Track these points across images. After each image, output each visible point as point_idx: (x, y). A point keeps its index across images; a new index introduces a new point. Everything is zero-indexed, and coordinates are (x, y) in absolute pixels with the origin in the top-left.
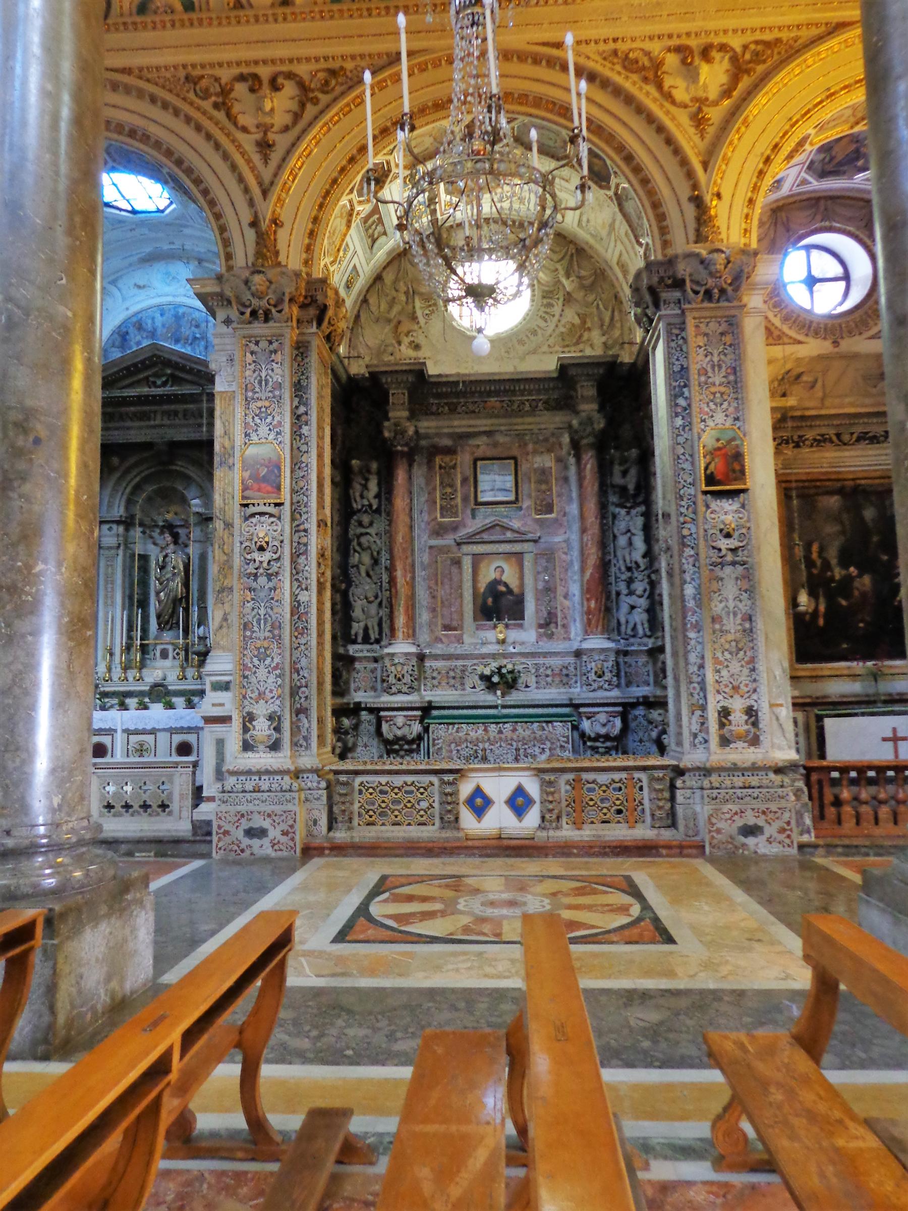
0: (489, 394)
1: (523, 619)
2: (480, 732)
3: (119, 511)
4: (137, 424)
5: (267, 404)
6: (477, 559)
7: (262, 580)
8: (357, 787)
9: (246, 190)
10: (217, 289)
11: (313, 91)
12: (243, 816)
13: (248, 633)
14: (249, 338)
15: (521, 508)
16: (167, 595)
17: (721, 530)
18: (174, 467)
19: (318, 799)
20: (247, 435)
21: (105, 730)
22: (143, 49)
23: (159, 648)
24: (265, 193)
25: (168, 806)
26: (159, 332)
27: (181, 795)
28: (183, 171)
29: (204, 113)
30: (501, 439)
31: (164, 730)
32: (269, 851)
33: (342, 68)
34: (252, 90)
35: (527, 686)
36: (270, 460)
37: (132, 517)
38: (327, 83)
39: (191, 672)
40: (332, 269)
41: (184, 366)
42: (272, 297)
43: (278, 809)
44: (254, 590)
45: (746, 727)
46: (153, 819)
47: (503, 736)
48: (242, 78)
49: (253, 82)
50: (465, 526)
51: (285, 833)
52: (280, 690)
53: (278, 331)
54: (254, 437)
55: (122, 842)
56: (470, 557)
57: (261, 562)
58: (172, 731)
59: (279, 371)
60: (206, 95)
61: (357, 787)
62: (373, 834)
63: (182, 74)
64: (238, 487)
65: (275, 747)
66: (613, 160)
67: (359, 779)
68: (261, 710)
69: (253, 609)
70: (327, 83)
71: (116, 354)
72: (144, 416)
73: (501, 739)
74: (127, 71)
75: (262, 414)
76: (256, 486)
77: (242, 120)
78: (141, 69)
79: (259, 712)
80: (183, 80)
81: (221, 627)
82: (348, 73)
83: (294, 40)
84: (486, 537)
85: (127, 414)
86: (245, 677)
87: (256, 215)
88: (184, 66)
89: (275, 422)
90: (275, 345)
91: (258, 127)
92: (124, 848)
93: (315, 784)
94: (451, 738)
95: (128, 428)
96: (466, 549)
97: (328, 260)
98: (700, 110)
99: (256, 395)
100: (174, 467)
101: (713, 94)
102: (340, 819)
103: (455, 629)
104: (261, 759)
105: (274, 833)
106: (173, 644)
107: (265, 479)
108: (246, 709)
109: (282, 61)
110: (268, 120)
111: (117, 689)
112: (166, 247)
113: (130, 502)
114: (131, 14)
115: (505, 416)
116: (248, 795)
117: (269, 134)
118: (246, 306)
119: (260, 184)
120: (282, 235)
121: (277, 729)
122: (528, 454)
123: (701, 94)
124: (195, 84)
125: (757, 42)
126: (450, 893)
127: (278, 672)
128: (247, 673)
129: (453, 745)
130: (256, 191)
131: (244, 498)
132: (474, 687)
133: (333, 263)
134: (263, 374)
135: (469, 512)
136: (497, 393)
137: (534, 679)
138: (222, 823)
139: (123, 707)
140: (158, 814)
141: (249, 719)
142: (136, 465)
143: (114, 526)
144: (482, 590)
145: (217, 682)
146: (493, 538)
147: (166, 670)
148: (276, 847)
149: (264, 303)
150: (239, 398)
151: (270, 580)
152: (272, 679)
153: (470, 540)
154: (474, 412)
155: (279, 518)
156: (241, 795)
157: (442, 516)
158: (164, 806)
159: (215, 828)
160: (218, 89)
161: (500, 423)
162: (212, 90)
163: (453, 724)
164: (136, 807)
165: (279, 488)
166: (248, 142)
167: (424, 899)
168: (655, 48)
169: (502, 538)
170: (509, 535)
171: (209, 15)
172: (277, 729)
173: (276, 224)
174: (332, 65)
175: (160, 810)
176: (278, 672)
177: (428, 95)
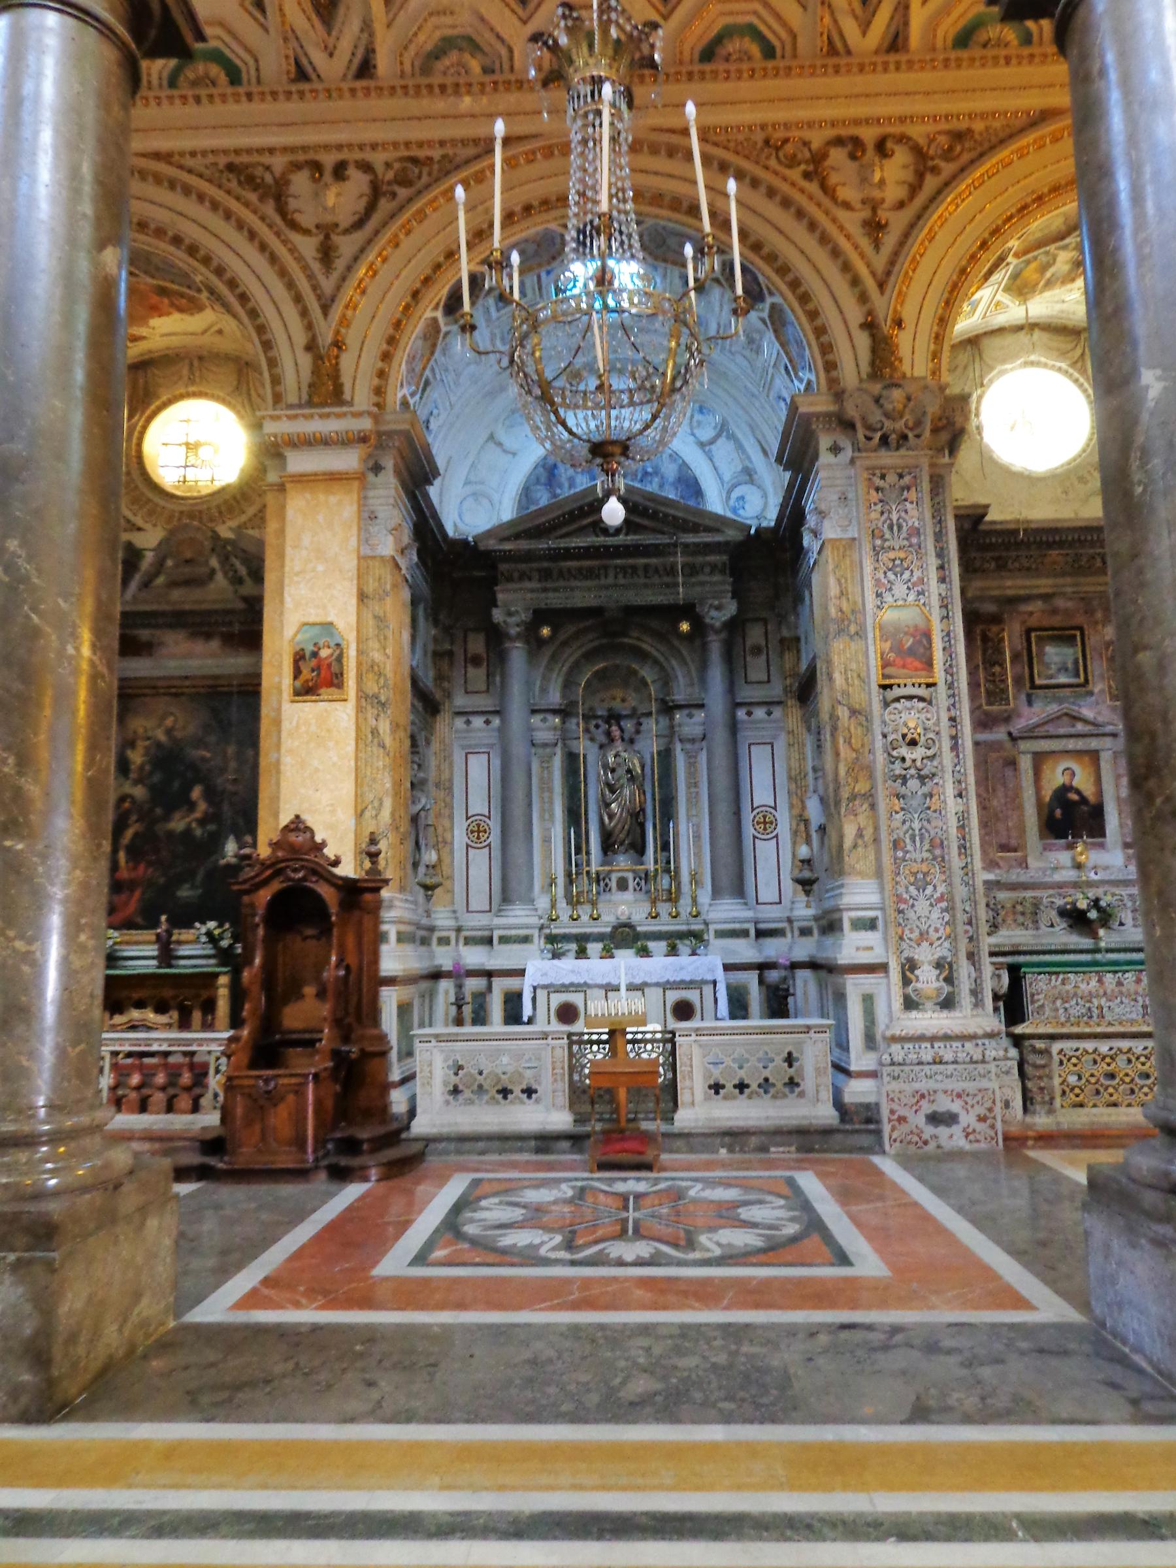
0: (1050, 545)
1: (1103, 835)
2: (1094, 983)
3: (555, 697)
5: (902, 555)
6: (1039, 759)
7: (913, 784)
8: (1056, 1058)
9: (855, 282)
10: (832, 408)
11: (932, 159)
12: (923, 1096)
13: (900, 854)
14: (871, 470)
15: (1091, 693)
16: (622, 807)
17: (904, 736)
18: (626, 640)
19: (1007, 1073)
20: (879, 595)
21: (579, 985)
23: (614, 877)
24: (325, 309)
27: (817, 1070)
28: (762, 258)
29: (793, 184)
30: (1060, 603)
31: (657, 984)
32: (961, 1142)
33: (970, 131)
34: (853, 157)
35: (1121, 924)
36: (916, 627)
37: (573, 704)
38: (951, 149)
39: (664, 908)
41: (646, 509)
42: (908, 417)
43: (970, 1086)
44: (903, 797)
45: (936, 985)
46: (778, 1102)
47: (1124, 989)
48: (839, 141)
49: (855, 146)
50: (1019, 716)
51: (982, 1119)
52: (948, 929)
53: (911, 462)
54: (888, 598)
55: (754, 1133)
56: (1029, 756)
57: (914, 761)
58: (667, 986)
59: (915, 513)
60: (792, 162)
61: (1056, 1058)
62: (1085, 1119)
63: (759, 137)
64: (874, 662)
65: (948, 1003)
66: (766, 274)
67: (1056, 1047)
68: (925, 955)
69: (904, 822)
70: (951, 149)
71: (543, 499)
72: (590, 574)
73: (1121, 993)
74: (157, 156)
75: (896, 568)
76: (899, 662)
77: (843, 193)
78: (182, 154)
79: (922, 958)
80: (760, 144)
81: (855, 846)
82: (977, 136)
84: (1051, 729)
85: (569, 570)
86: (900, 912)
87: (870, 313)
88: (763, 127)
89: (915, 579)
90: (907, 480)
91: (863, 202)
92: (754, 1141)
93: (1001, 1053)
94: (1056, 992)
96: (1024, 745)
98: (327, 237)
99: (887, 544)
100: (626, 640)
101: (345, 219)
102: (1039, 1099)
103: (1015, 850)
104: (930, 1021)
105: (967, 1119)
106: (634, 871)
107: (911, 651)
108: (905, 954)
109: (350, 146)
110: (876, 194)
111: (567, 931)
113: (568, 685)
114: (691, 61)
115: (1070, 575)
116: (927, 1068)
117: (879, 212)
118: (875, 430)
119: (873, 274)
120: (346, 362)
121: (949, 980)
122: (1096, 623)
123: (329, 218)
124: (777, 149)
125: (402, 159)
127: (944, 904)
128: (902, 906)
129: (1059, 1003)
130: (870, 284)
131: (884, 676)
132: (1052, 926)
134: (895, 517)
135: (1023, 697)
136: (1061, 544)
137: (1130, 915)
138: (895, 1107)
139: (582, 954)
140: (785, 1096)
141: (910, 966)
142: (576, 636)
143: (550, 717)
144: (1047, 799)
145: (859, 919)
146: (1062, 731)
147: (626, 906)
148: (971, 1137)
149: (900, 425)
150: (867, 548)
151: (923, 784)
152: (936, 914)
153: (1030, 734)
154: (1028, 569)
155: (930, 703)
156: (917, 1068)
157: (989, 703)
158: (529, 1092)
159: (885, 1113)
160: (807, 155)
161: (1067, 584)
162: (800, 156)
163: (1057, 973)
164: (754, 1086)
165: (929, 664)
166: (852, 221)
168: (279, 163)
169: (1072, 731)
170: (1080, 727)
172: (949, 980)
173: (340, 348)
174: (955, 125)
175: (787, 1090)
176: (944, 904)
177: (533, 192)
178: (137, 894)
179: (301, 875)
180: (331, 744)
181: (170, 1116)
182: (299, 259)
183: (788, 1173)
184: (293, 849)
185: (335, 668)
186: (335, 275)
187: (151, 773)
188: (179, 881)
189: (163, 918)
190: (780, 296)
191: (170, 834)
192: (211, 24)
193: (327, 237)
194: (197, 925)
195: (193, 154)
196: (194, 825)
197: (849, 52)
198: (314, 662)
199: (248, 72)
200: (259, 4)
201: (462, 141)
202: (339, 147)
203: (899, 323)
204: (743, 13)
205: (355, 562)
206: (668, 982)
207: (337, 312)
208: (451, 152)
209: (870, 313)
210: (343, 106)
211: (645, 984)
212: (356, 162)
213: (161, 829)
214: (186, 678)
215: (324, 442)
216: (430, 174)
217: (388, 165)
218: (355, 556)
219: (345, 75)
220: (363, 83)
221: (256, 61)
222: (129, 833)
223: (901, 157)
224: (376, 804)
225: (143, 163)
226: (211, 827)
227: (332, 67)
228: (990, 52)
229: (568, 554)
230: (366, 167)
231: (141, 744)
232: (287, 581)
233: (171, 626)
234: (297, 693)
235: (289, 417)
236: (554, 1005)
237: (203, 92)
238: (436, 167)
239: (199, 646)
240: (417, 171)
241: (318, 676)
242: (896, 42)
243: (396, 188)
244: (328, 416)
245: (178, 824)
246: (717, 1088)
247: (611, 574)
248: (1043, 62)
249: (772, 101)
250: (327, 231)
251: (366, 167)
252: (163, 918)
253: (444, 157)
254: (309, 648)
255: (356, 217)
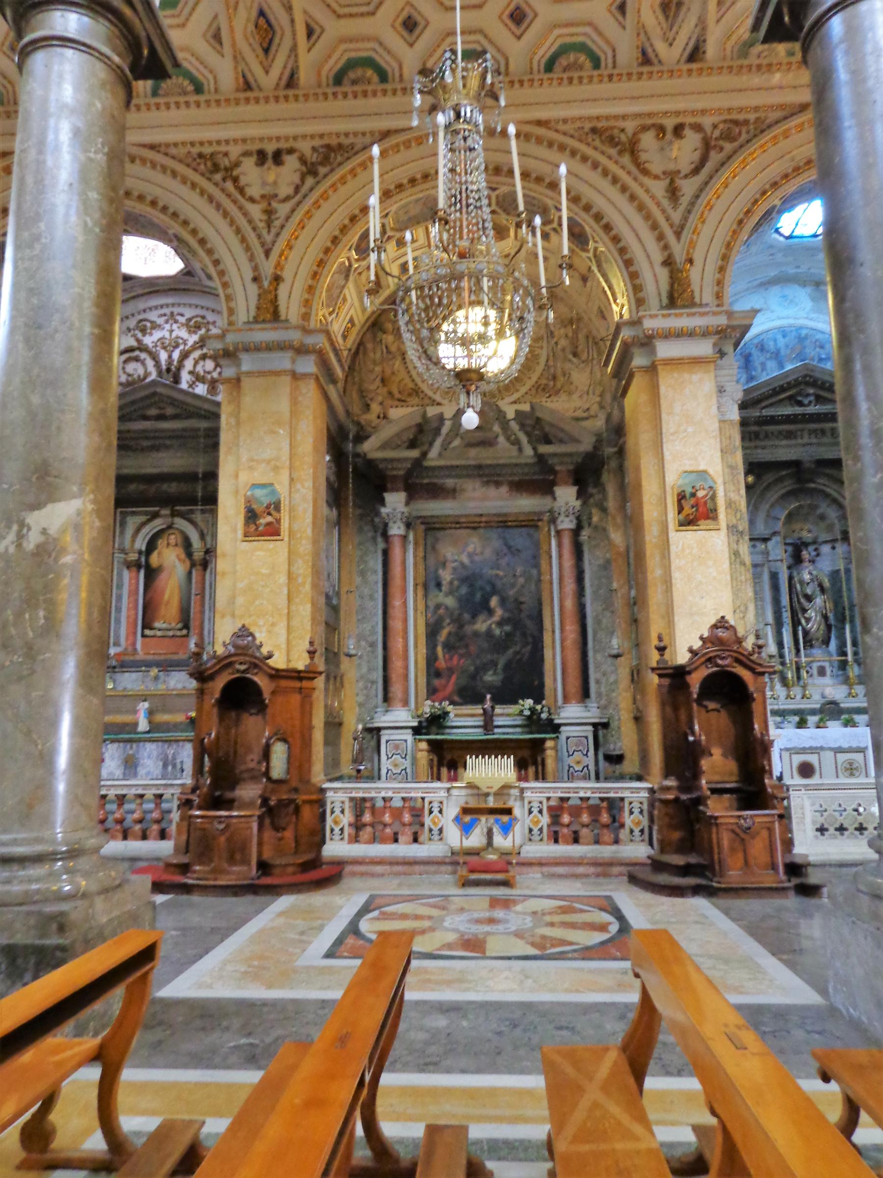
4: (784, 442)
18: (813, 485)
21: (816, 748)
22: (243, 122)
23: (815, 666)
24: (267, 253)
25: (817, 830)
26: (783, 352)
31: (831, 749)
40: (330, 319)
48: (246, 154)
66: (589, 226)
72: (790, 435)
78: (167, 145)
83: (740, 90)
95: (776, 446)
97: (326, 311)
98: (672, 181)
101: (685, 166)
112: (792, 271)
119: (263, 244)
120: (283, 291)
123: (672, 167)
125: (725, 121)
126: (435, 912)
133: (330, 314)
167: (417, 917)
171: (166, 100)
178: (454, 678)
179: (727, 662)
180: (710, 563)
181: (416, 846)
182: (653, 197)
183: (608, 893)
184: (719, 642)
185: (710, 505)
186: (682, 208)
187: (458, 587)
188: (483, 668)
189: (488, 696)
190: (600, 244)
191: (476, 634)
192: (182, 50)
193: (672, 181)
194: (521, 701)
195: (176, 145)
196: (493, 626)
197: (260, 89)
198: (693, 501)
199: (606, 58)
200: (622, 8)
201: (693, 112)
202: (677, 113)
203: (691, 261)
204: (368, 50)
205: (717, 425)
206: (840, 747)
207: (686, 234)
208: (763, 115)
209: (670, 256)
210: (273, 109)
211: (822, 748)
212: (690, 124)
213: (469, 629)
214: (481, 515)
215: (690, 334)
216: (748, 132)
217: (715, 126)
218: (716, 421)
219: (278, 84)
220: (694, 66)
221: (614, 51)
222: (444, 633)
223: (291, 162)
224: (742, 608)
225: (134, 150)
226: (508, 628)
227: (669, 54)
228: (358, 88)
229: (772, 420)
230: (697, 128)
231: (450, 565)
232: (664, 440)
233: (468, 476)
234: (681, 524)
235: (664, 316)
236: (795, 765)
237: (576, 75)
238: (752, 127)
239: (492, 491)
240: (737, 130)
241: (695, 510)
242: (695, 54)
243: (721, 143)
244: (693, 314)
245: (482, 625)
246: (822, 830)
247: (806, 435)
248: (709, 75)
249: (201, 125)
250: (672, 176)
251: (697, 128)
252: (488, 696)
253: (757, 119)
254: (689, 490)
255: (693, 166)
